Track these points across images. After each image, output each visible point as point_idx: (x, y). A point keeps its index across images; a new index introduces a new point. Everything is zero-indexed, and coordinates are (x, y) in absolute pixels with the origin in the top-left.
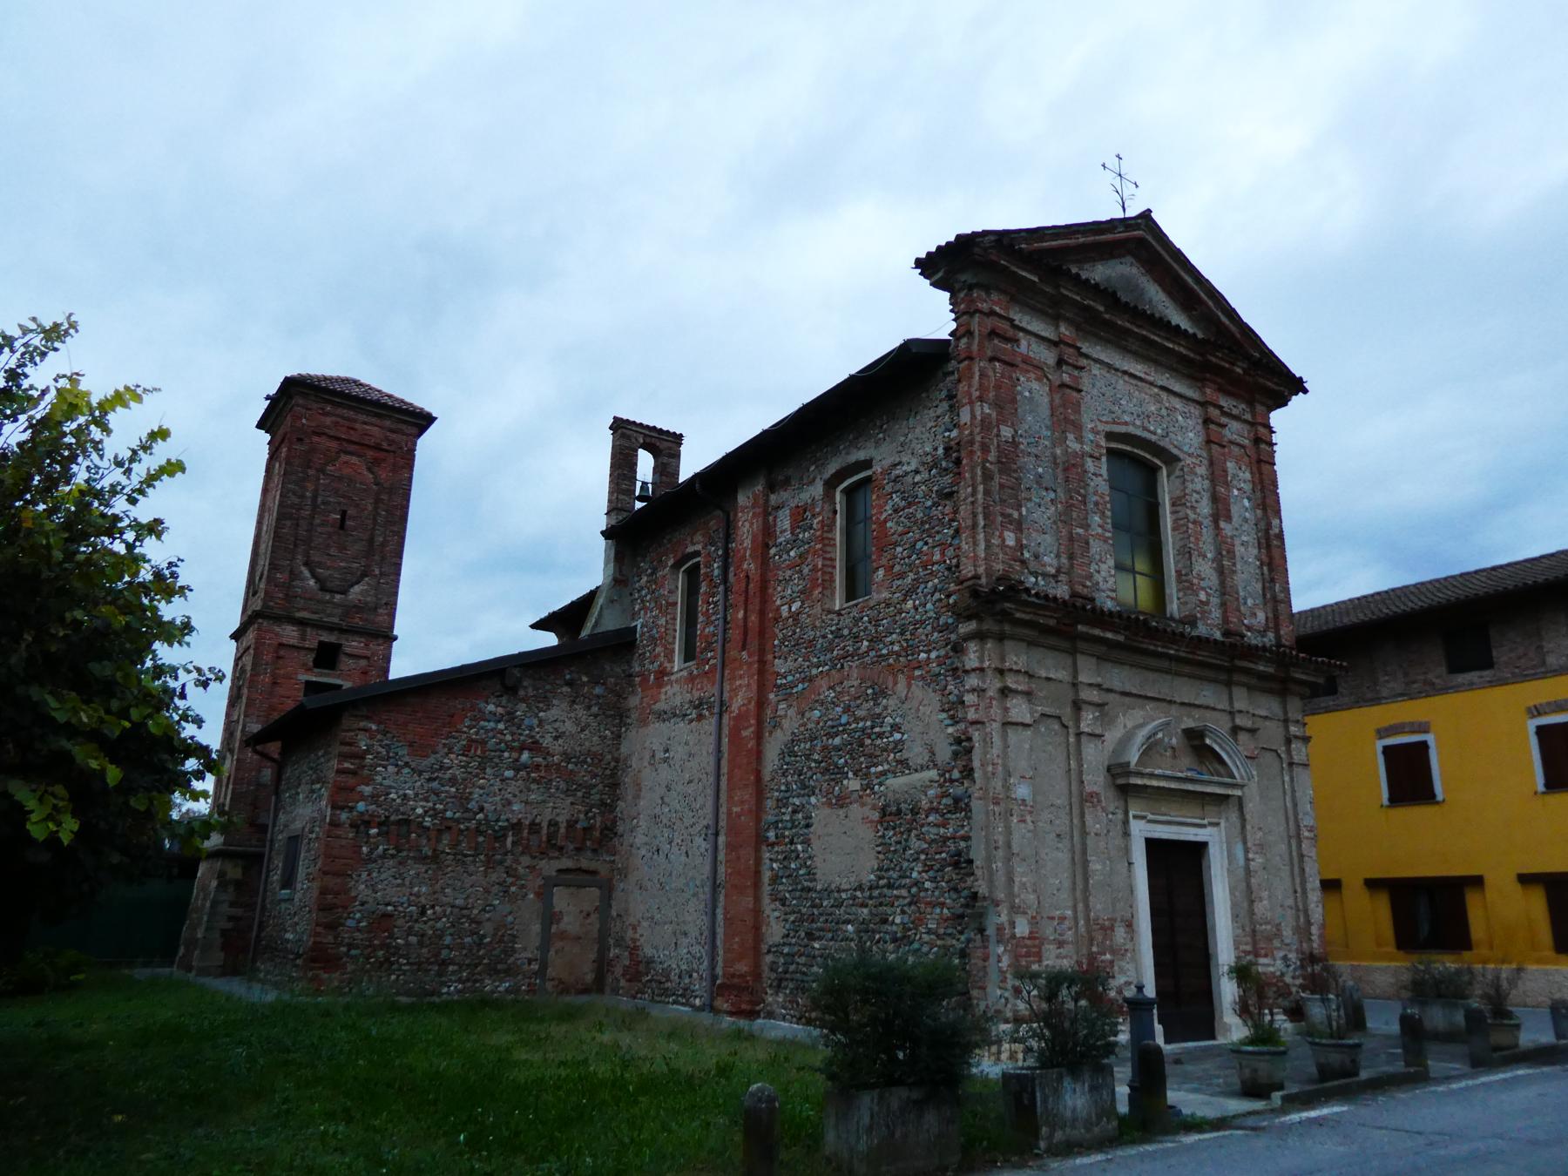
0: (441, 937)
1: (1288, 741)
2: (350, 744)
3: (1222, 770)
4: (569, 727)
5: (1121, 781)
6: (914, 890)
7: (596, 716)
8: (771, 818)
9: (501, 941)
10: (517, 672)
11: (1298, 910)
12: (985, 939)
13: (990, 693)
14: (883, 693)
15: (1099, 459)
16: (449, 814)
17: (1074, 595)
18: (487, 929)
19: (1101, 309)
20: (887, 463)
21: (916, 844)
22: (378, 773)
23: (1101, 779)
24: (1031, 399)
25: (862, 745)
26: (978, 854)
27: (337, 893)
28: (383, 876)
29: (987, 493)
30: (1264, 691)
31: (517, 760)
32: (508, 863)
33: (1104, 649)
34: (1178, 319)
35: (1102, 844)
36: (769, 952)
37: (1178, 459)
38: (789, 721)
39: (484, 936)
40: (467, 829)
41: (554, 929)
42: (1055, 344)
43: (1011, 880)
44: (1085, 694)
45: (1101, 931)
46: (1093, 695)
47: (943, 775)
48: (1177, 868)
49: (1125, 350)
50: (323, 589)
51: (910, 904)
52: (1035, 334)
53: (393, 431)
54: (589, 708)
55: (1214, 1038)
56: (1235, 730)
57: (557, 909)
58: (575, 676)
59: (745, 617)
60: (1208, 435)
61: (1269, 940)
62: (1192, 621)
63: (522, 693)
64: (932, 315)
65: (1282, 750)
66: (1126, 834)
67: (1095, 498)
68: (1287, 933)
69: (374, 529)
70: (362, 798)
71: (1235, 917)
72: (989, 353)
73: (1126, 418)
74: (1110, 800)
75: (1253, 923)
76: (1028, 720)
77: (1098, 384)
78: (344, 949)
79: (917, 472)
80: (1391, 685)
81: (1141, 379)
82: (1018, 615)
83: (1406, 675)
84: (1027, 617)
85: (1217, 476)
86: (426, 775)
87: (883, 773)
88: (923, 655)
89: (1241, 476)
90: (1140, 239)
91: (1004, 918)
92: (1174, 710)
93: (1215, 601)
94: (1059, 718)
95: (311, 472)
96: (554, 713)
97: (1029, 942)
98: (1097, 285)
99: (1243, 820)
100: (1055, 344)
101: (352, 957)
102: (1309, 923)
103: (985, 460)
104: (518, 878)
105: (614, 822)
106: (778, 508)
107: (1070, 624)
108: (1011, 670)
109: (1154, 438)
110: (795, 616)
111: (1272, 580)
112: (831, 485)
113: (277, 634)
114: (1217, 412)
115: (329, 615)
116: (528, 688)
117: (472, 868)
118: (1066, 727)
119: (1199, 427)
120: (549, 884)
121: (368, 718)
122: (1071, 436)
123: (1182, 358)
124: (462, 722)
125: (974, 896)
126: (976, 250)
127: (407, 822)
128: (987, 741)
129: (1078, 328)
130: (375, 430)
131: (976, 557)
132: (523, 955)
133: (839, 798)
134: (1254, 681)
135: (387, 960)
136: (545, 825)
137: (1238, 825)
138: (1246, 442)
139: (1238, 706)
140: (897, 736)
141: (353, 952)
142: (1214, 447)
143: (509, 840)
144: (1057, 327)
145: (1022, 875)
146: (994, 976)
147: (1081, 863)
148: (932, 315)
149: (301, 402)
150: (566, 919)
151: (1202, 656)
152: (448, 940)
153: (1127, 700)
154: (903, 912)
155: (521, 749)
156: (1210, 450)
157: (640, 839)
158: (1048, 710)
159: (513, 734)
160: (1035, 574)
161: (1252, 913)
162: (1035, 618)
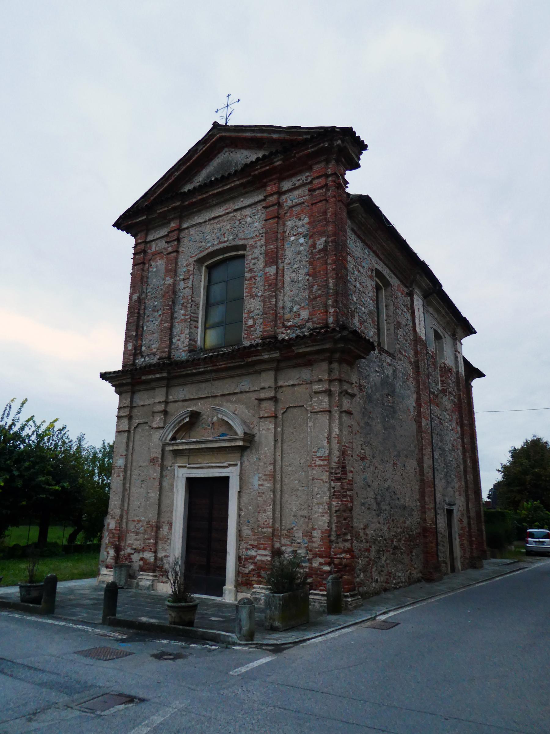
48: (207, 497)
90: (221, 138)
94: (147, 423)
151: (222, 364)
158: (141, 421)
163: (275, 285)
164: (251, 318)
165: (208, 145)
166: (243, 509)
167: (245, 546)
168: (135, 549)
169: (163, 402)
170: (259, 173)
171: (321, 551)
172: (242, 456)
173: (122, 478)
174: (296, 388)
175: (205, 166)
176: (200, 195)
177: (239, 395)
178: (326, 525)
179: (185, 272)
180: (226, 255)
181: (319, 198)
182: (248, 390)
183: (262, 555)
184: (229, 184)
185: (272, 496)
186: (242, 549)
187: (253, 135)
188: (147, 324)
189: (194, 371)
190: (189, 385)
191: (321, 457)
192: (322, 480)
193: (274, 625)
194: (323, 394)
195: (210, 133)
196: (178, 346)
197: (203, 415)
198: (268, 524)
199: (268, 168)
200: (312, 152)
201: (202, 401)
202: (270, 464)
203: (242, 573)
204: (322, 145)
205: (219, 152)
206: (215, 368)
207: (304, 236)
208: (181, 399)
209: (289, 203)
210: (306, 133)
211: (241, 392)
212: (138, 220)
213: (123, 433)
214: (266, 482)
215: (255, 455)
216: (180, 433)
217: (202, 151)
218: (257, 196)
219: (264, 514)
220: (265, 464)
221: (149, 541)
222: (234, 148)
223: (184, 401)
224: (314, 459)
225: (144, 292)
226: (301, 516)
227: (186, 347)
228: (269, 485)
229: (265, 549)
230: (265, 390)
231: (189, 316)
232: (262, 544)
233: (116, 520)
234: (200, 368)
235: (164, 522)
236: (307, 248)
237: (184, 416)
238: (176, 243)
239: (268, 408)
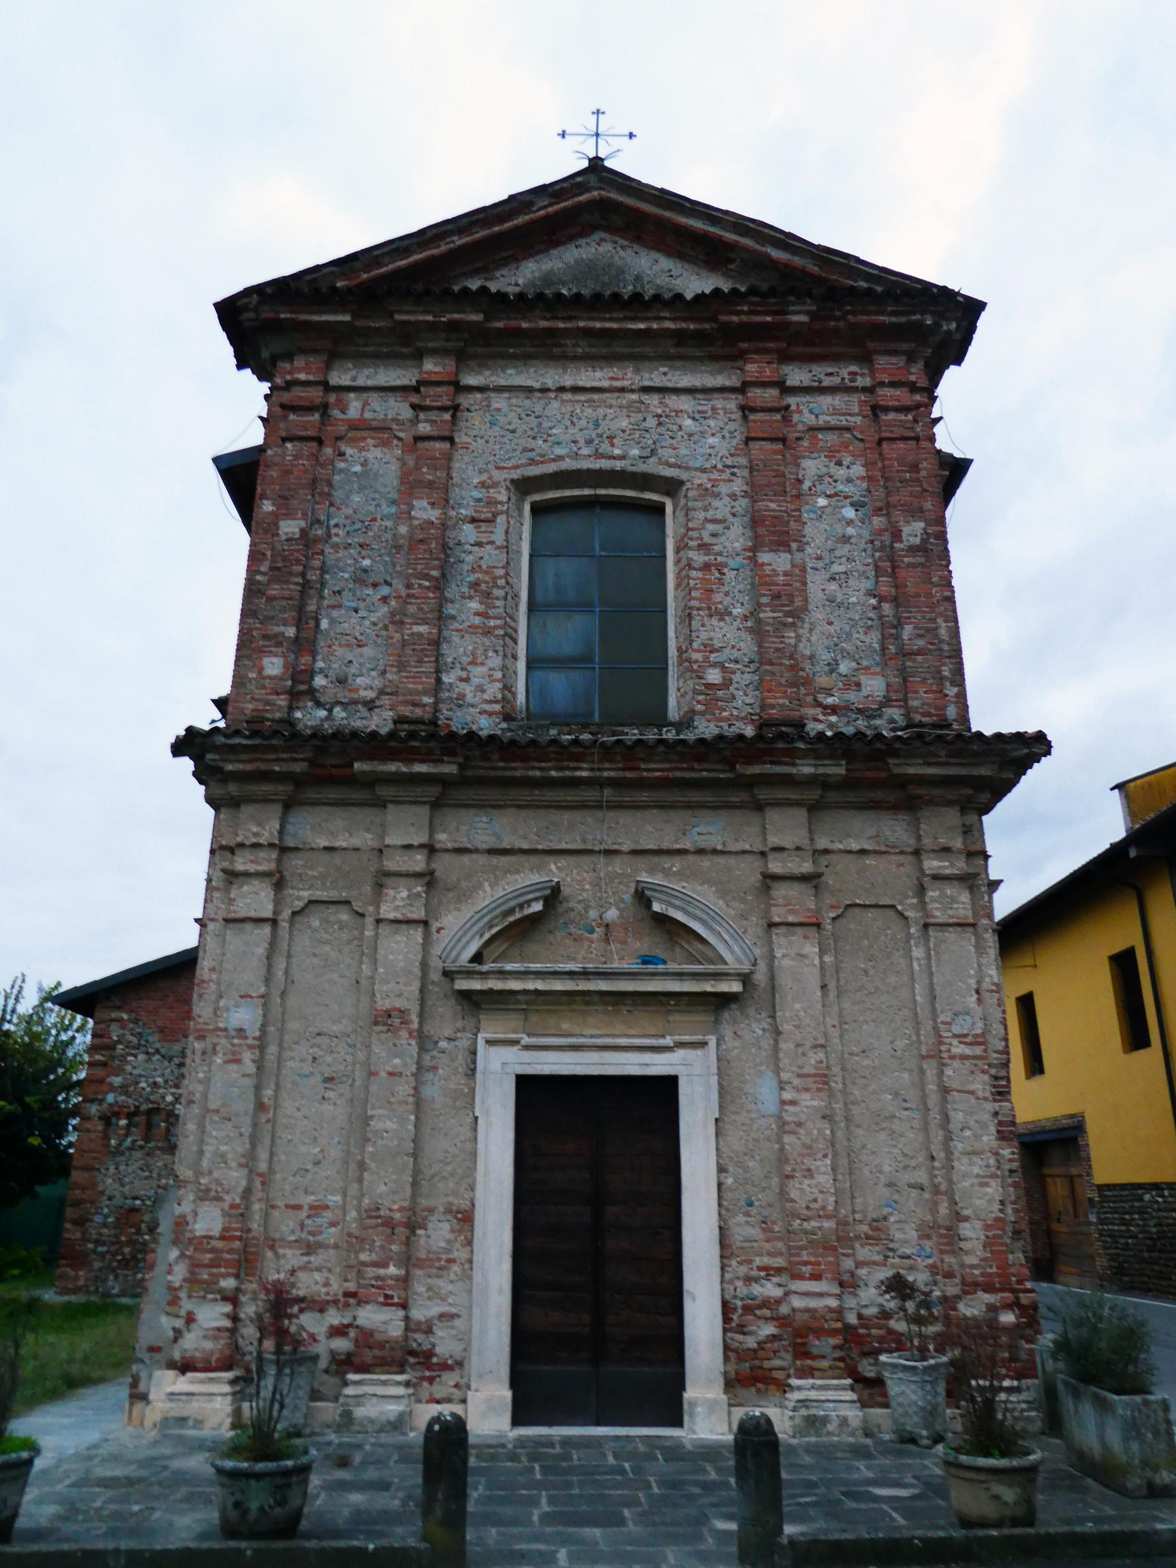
1: (921, 890)
11: (936, 1190)
22: (128, 1062)
27: (84, 1188)
28: (130, 1169)
30: (862, 807)
37: (681, 483)
49: (565, 359)
55: (678, 1422)
67: (472, 578)
70: (112, 1089)
73: (559, 451)
82: (230, 767)
84: (249, 767)
90: (598, 202)
91: (186, 1208)
92: (617, 865)
93: (742, 678)
94: (348, 903)
97: (219, 1244)
98: (521, 296)
111: (899, 625)
121: (120, 1008)
123: (680, 337)
134: (814, 794)
135: (134, 1257)
141: (100, 1249)
151: (654, 770)
153: (504, 860)
162: (263, 767)
163: (783, 602)
164: (715, 665)
165: (563, 205)
166: (731, 1169)
167: (743, 1270)
169: (421, 846)
170: (741, 325)
171: (990, 1275)
172: (717, 1022)
173: (251, 1068)
174: (870, 861)
175: (537, 253)
176: (545, 318)
177: (691, 858)
178: (996, 1206)
179: (479, 500)
180: (603, 492)
181: (898, 432)
182: (719, 847)
184: (643, 320)
185: (828, 1132)
186: (731, 1282)
187: (712, 229)
188: (335, 613)
189: (553, 773)
190: (512, 812)
191: (965, 1036)
192: (972, 1093)
193: (1158, 1481)
194: (955, 883)
195: (579, 179)
196: (462, 696)
197: (566, 900)
198: (823, 1208)
199: (769, 319)
200: (892, 324)
201: (563, 862)
202: (816, 1046)
203: (735, 1351)
204: (918, 317)
205: (581, 235)
206: (629, 775)
207: (857, 506)
208: (485, 846)
209: (809, 419)
210: (868, 277)
211: (701, 852)
212: (316, 318)
213: (248, 926)
214: (807, 1096)
215: (757, 1020)
216: (497, 943)
217: (542, 213)
218: (712, 374)
219: (807, 1182)
220: (798, 1046)
221: (382, 1271)
222: (632, 241)
223: (492, 852)
224: (947, 1040)
225: (318, 521)
226: (910, 1186)
227: (491, 702)
228: (815, 1103)
229: (816, 1277)
230: (785, 854)
231: (498, 622)
232: (806, 1263)
233: (226, 1206)
234: (576, 769)
235: (431, 1211)
236: (866, 534)
237: (531, 896)
238: (447, 416)
239: (790, 901)
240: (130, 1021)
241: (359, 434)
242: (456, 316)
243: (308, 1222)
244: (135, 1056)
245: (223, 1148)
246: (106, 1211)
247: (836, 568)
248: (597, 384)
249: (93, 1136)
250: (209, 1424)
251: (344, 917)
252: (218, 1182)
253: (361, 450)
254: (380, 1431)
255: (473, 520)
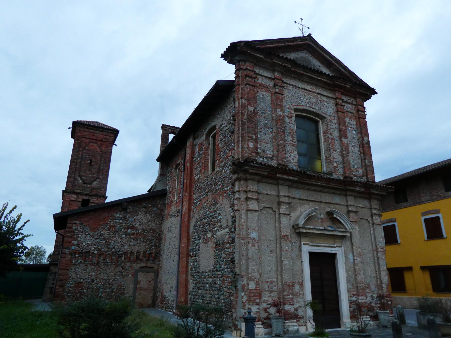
0: (99, 289)
1: (372, 216)
2: (70, 228)
3: (342, 226)
4: (144, 221)
5: (297, 231)
6: (223, 272)
7: (154, 217)
8: (191, 248)
9: (119, 290)
10: (126, 204)
11: (377, 278)
12: (237, 290)
13: (242, 200)
14: (217, 203)
15: (291, 118)
16: (103, 249)
17: (279, 164)
18: (115, 287)
19: (290, 66)
20: (219, 125)
21: (224, 255)
23: (289, 230)
24: (263, 98)
25: (212, 221)
26: (237, 259)
27: (64, 276)
28: (79, 270)
29: (243, 129)
30: (361, 198)
31: (126, 232)
32: (123, 265)
33: (290, 183)
34: (326, 71)
35: (289, 254)
36: (190, 294)
37: (325, 118)
38: (196, 214)
39: (114, 289)
40: (109, 254)
41: (138, 286)
42: (273, 79)
43: (248, 268)
44: (282, 199)
45: (290, 287)
46: (287, 200)
47: (230, 230)
48: (323, 266)
49: (303, 81)
50: (84, 183)
51: (222, 277)
52: (264, 76)
53: (106, 136)
54: (151, 215)
55: (340, 327)
56: (349, 212)
57: (139, 280)
58: (147, 205)
59: (187, 181)
60: (337, 109)
61: (364, 290)
62: (331, 174)
63: (128, 210)
64: (228, 72)
65: (370, 219)
66: (300, 250)
67: (289, 131)
68: (373, 287)
69: (100, 165)
70: (74, 245)
71: (348, 281)
72: (246, 83)
73: (303, 104)
74: (294, 239)
75: (357, 283)
76: (257, 209)
77: (291, 93)
78: (66, 294)
79: (226, 126)
80: (425, 197)
81: (309, 91)
82: (251, 171)
83: (431, 193)
84: (255, 172)
85: (341, 123)
86: (95, 237)
87: (216, 231)
88: (226, 188)
89: (351, 123)
90: (307, 44)
91: (245, 282)
92: (322, 205)
93: (340, 166)
94: (272, 208)
95: (81, 149)
96: (139, 216)
97: (255, 291)
99: (352, 245)
100: (273, 79)
101: (68, 296)
102: (382, 283)
103: (242, 118)
104: (126, 270)
105: (160, 251)
106: (196, 145)
107: (274, 174)
108: (250, 191)
109: (314, 110)
110: (198, 179)
111: (365, 159)
112: (208, 135)
113: (69, 197)
114: (341, 101)
115: (86, 191)
116: (130, 209)
117: (110, 267)
118: (275, 212)
119: (333, 107)
120: (137, 271)
122: (278, 110)
123: (326, 83)
124: (108, 220)
125: (236, 274)
126: (238, 48)
127: (89, 252)
128: (240, 217)
129: (282, 74)
130: (100, 135)
131: (238, 152)
132: (127, 295)
133: (206, 240)
134: (356, 194)
135: (80, 297)
136: (135, 252)
137: (350, 247)
138: (354, 111)
139: (349, 203)
140: (220, 217)
142: (339, 113)
143: (123, 257)
144: (274, 73)
145: (253, 266)
146: (240, 304)
147: (280, 263)
148: (228, 72)
149: (78, 128)
150: (142, 283)
151: (332, 185)
152: (101, 290)
153: (302, 202)
154: (220, 280)
155: (128, 228)
156: (338, 114)
157: (164, 256)
158: (267, 206)
159: (125, 224)
160: (263, 158)
161: (356, 279)
162: (258, 172)
164: (335, 162)
168: (270, 304)
174: (363, 209)
180: (308, 115)
183: (361, 299)
188: (261, 133)
196: (290, 160)
201: (313, 203)
206: (328, 185)
212: (256, 54)
213: (253, 212)
221: (289, 297)
229: (362, 296)
240: (79, 224)
241: (261, 87)
242: (286, 64)
243: (270, 286)
244: (82, 235)
245: (253, 267)
246: (71, 283)
247: (353, 144)
248: (308, 89)
249: (67, 259)
250: (260, 334)
251: (271, 211)
252: (253, 276)
253: (262, 91)
254: (294, 333)
255: (288, 117)
